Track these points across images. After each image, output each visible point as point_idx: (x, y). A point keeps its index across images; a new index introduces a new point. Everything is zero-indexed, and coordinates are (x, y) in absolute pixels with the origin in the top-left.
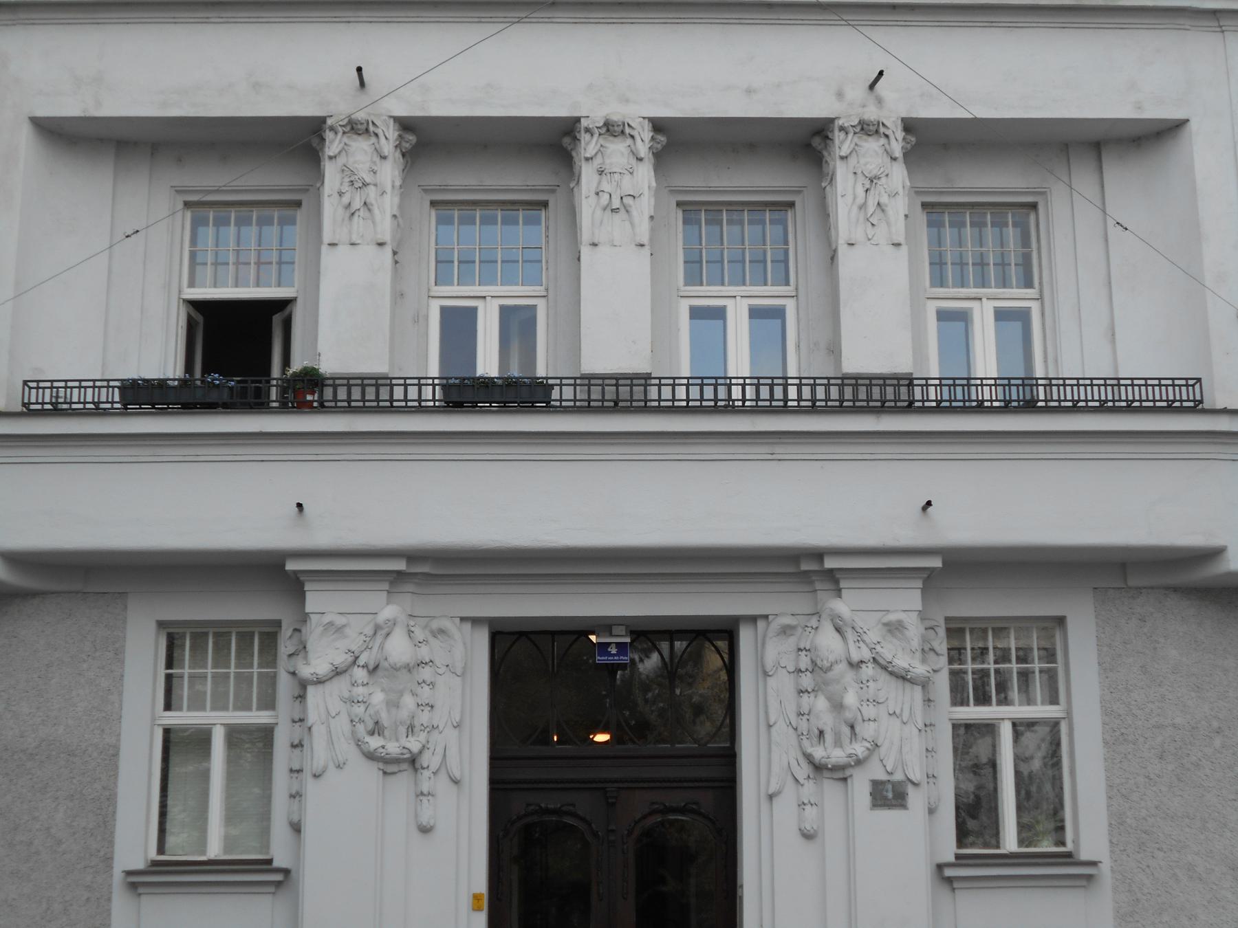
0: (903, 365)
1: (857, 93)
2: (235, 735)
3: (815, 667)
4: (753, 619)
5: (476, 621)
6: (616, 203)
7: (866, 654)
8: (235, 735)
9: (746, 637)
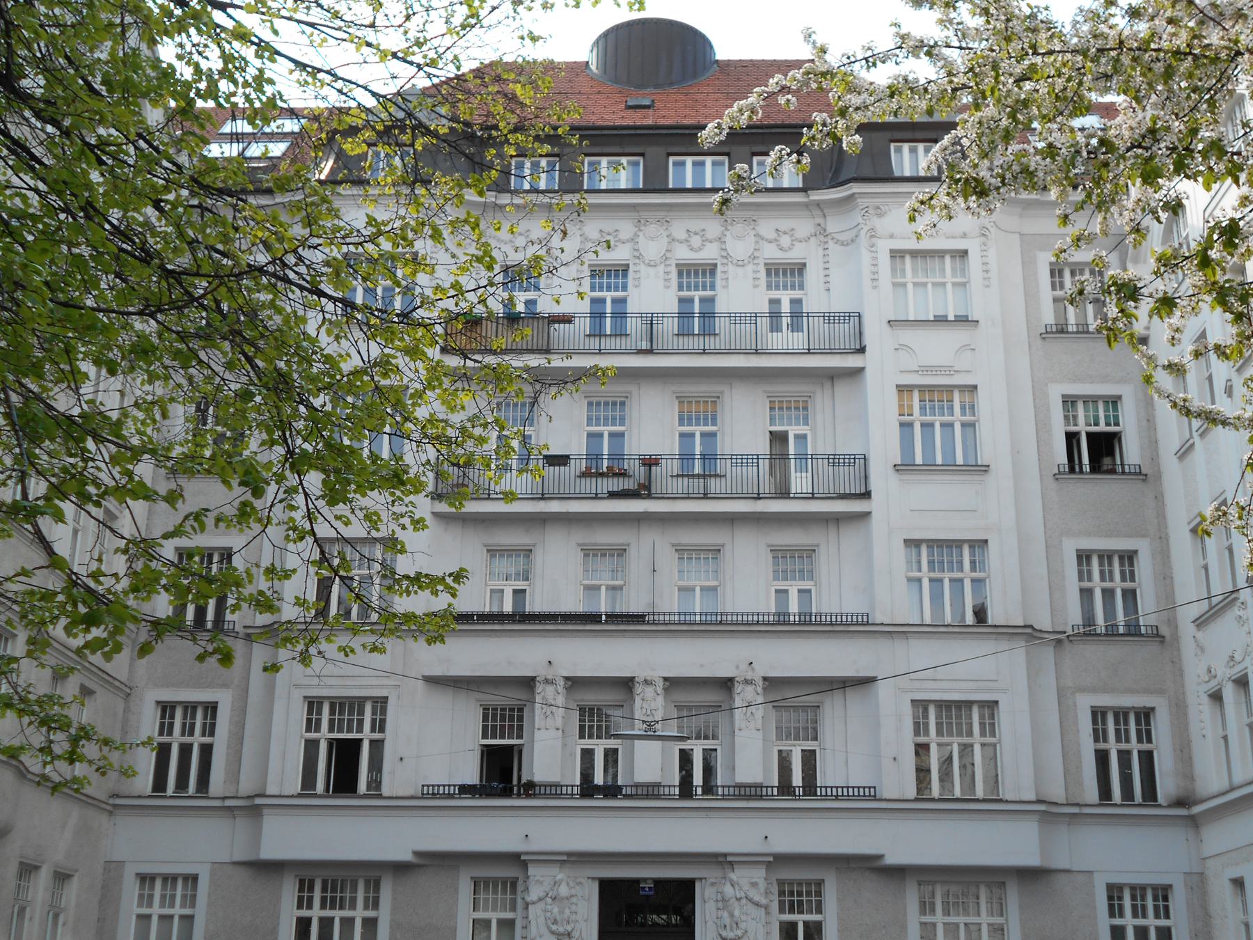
0: (758, 779)
1: (744, 666)
2: (501, 922)
3: (723, 900)
4: (701, 879)
5: (593, 879)
6: (649, 713)
7: (743, 895)
8: (501, 922)
9: (698, 886)
